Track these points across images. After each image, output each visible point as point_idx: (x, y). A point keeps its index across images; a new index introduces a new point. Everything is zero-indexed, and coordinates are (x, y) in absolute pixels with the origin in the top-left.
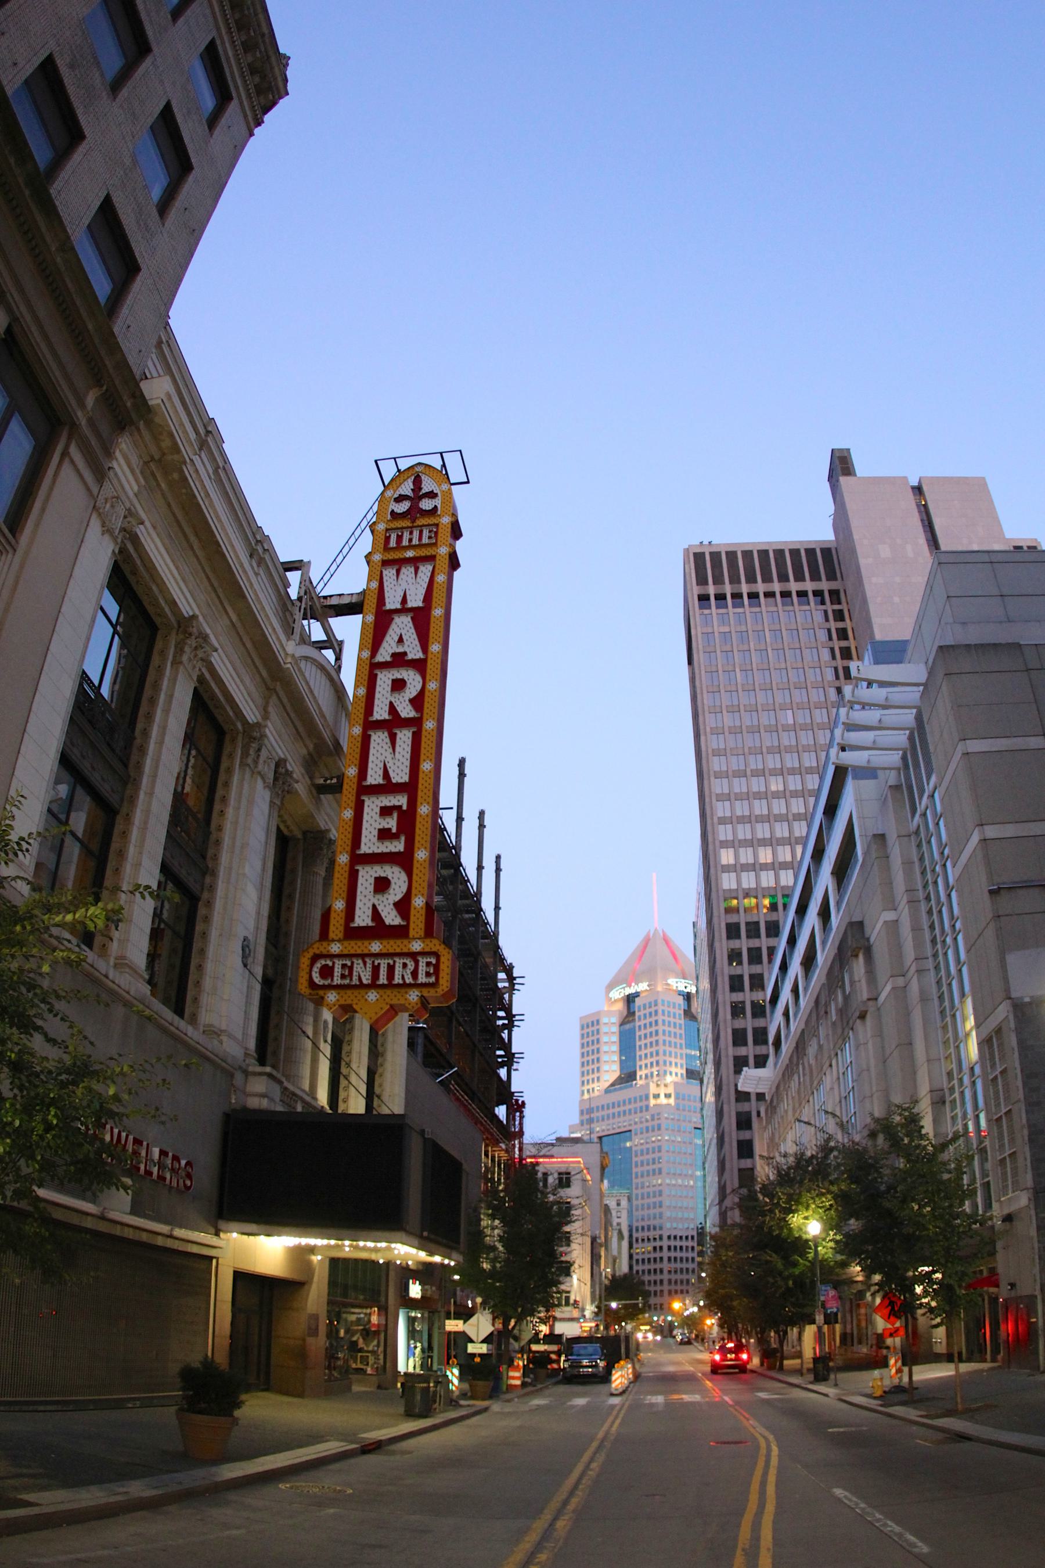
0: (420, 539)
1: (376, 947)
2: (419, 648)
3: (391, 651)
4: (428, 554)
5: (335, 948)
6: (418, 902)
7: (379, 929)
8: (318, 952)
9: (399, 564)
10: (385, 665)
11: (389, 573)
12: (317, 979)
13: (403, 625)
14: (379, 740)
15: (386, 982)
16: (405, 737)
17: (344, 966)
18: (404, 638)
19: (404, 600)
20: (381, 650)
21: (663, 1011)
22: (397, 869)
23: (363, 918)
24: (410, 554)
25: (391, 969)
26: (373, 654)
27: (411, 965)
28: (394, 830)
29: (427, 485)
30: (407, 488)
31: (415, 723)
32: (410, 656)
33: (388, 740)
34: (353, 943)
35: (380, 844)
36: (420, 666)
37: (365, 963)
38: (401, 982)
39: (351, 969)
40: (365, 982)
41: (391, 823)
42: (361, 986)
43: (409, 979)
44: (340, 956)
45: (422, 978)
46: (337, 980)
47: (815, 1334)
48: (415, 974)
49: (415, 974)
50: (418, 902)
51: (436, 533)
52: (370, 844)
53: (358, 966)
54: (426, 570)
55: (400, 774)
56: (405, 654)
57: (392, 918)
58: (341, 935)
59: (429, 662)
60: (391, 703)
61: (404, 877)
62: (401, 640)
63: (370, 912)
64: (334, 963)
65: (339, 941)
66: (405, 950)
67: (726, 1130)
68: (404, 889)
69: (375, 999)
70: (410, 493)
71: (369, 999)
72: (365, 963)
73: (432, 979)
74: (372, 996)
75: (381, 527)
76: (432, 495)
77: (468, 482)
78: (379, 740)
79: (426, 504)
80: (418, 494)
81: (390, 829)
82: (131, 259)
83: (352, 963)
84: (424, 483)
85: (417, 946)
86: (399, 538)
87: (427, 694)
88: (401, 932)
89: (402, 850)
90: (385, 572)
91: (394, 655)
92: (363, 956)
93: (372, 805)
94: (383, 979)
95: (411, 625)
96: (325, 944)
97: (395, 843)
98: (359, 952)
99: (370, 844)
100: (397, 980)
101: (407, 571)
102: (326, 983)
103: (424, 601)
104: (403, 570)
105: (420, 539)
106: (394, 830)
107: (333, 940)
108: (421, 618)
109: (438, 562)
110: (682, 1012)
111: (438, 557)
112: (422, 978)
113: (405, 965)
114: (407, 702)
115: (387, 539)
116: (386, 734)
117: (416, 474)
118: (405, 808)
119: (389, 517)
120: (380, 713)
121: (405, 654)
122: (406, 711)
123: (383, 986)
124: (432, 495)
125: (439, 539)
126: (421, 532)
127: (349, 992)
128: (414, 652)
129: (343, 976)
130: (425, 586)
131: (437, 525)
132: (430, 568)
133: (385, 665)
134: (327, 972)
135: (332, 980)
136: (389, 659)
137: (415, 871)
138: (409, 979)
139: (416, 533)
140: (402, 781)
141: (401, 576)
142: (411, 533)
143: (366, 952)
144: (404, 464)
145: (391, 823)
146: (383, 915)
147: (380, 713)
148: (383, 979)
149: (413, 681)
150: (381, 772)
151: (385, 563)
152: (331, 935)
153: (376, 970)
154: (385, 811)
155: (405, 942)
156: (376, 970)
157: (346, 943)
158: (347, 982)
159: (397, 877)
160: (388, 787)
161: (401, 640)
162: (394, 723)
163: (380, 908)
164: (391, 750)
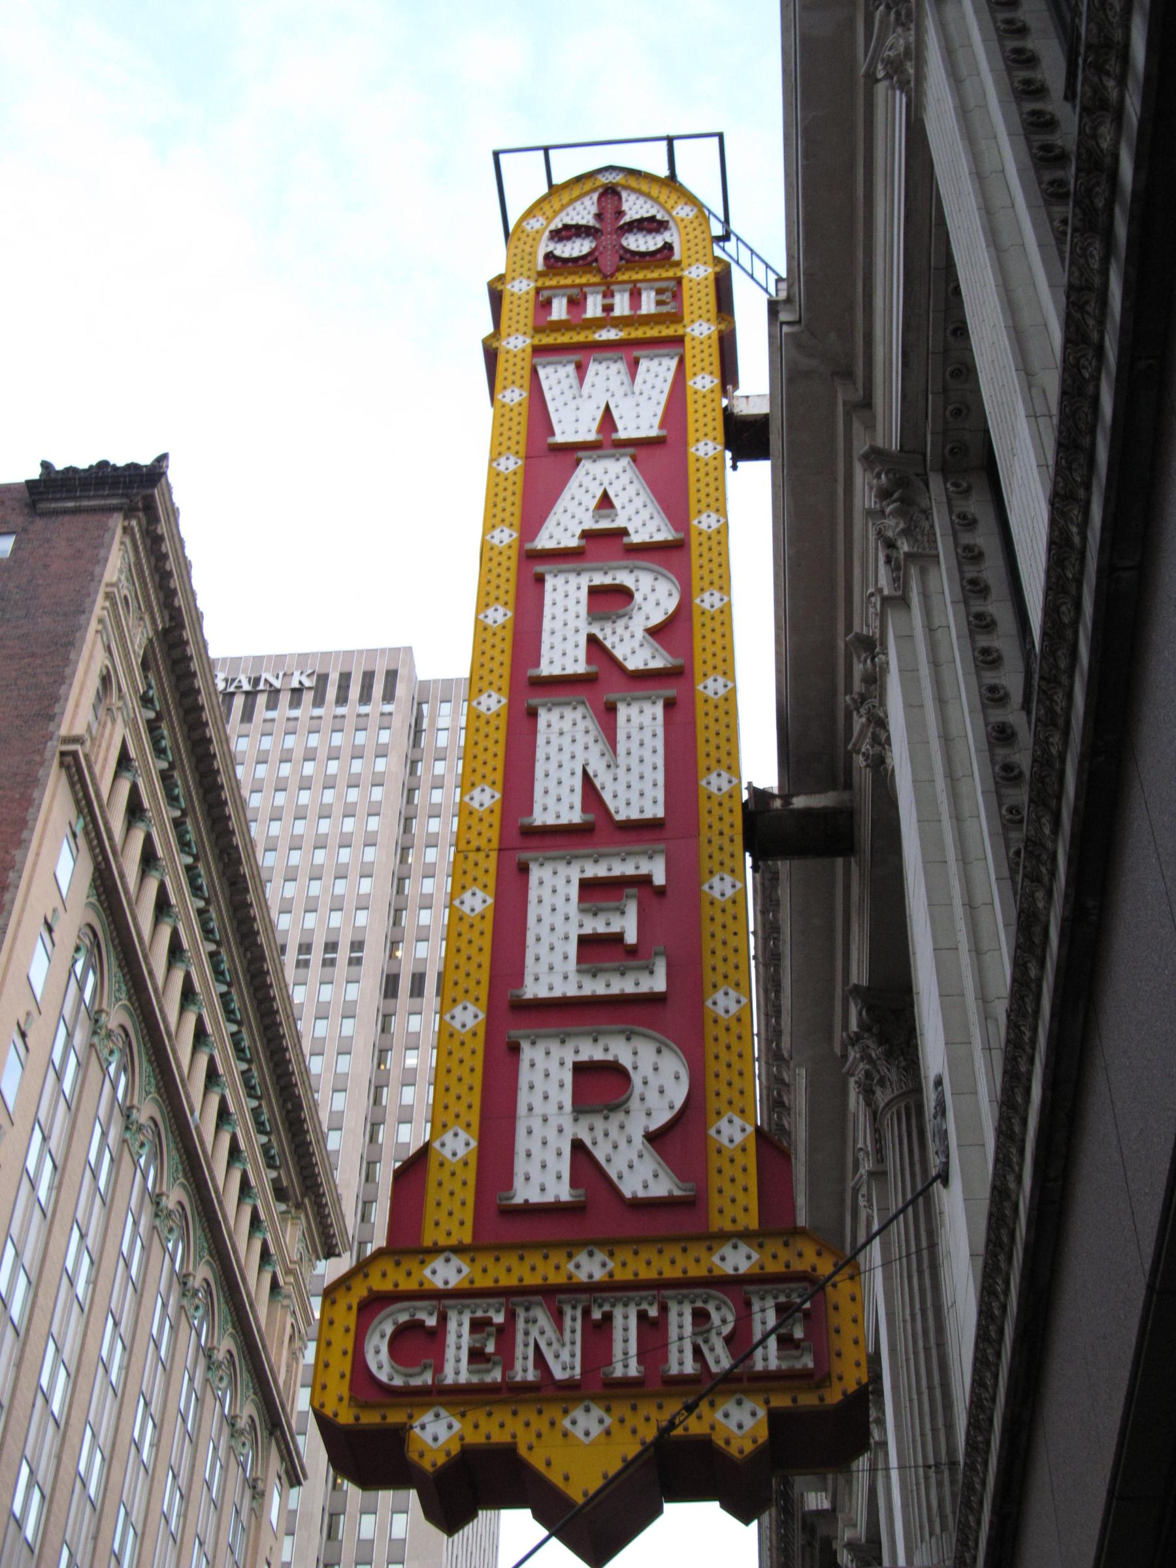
1: (590, 1267)
5: (445, 1273)
6: (732, 1132)
12: (380, 1362)
15: (633, 1370)
26: (533, 515)
27: (723, 1319)
28: (631, 938)
29: (635, 207)
33: (591, 724)
36: (669, 555)
37: (558, 1318)
39: (505, 1334)
40: (559, 1374)
46: (457, 1368)
50: (732, 1132)
52: (552, 971)
55: (637, 793)
57: (640, 1175)
74: (587, 1422)
77: (720, 136)
80: (610, 221)
82: (84, 471)
85: (736, 1260)
88: (677, 1218)
90: (542, 373)
92: (554, 1296)
94: (626, 1362)
96: (409, 1263)
99: (552, 971)
100: (681, 1362)
106: (631, 938)
112: (769, 1358)
113: (700, 1316)
117: (608, 187)
120: (563, 653)
122: (633, 649)
123: (514, 760)
135: (439, 1369)
136: (574, 543)
138: (720, 1359)
143: (555, 1279)
144: (566, 167)
148: (626, 1362)
149: (655, 597)
153: (598, 1334)
157: (486, 1260)
158: (496, 1375)
159: (659, 1080)
160: (597, 828)
162: (600, 686)
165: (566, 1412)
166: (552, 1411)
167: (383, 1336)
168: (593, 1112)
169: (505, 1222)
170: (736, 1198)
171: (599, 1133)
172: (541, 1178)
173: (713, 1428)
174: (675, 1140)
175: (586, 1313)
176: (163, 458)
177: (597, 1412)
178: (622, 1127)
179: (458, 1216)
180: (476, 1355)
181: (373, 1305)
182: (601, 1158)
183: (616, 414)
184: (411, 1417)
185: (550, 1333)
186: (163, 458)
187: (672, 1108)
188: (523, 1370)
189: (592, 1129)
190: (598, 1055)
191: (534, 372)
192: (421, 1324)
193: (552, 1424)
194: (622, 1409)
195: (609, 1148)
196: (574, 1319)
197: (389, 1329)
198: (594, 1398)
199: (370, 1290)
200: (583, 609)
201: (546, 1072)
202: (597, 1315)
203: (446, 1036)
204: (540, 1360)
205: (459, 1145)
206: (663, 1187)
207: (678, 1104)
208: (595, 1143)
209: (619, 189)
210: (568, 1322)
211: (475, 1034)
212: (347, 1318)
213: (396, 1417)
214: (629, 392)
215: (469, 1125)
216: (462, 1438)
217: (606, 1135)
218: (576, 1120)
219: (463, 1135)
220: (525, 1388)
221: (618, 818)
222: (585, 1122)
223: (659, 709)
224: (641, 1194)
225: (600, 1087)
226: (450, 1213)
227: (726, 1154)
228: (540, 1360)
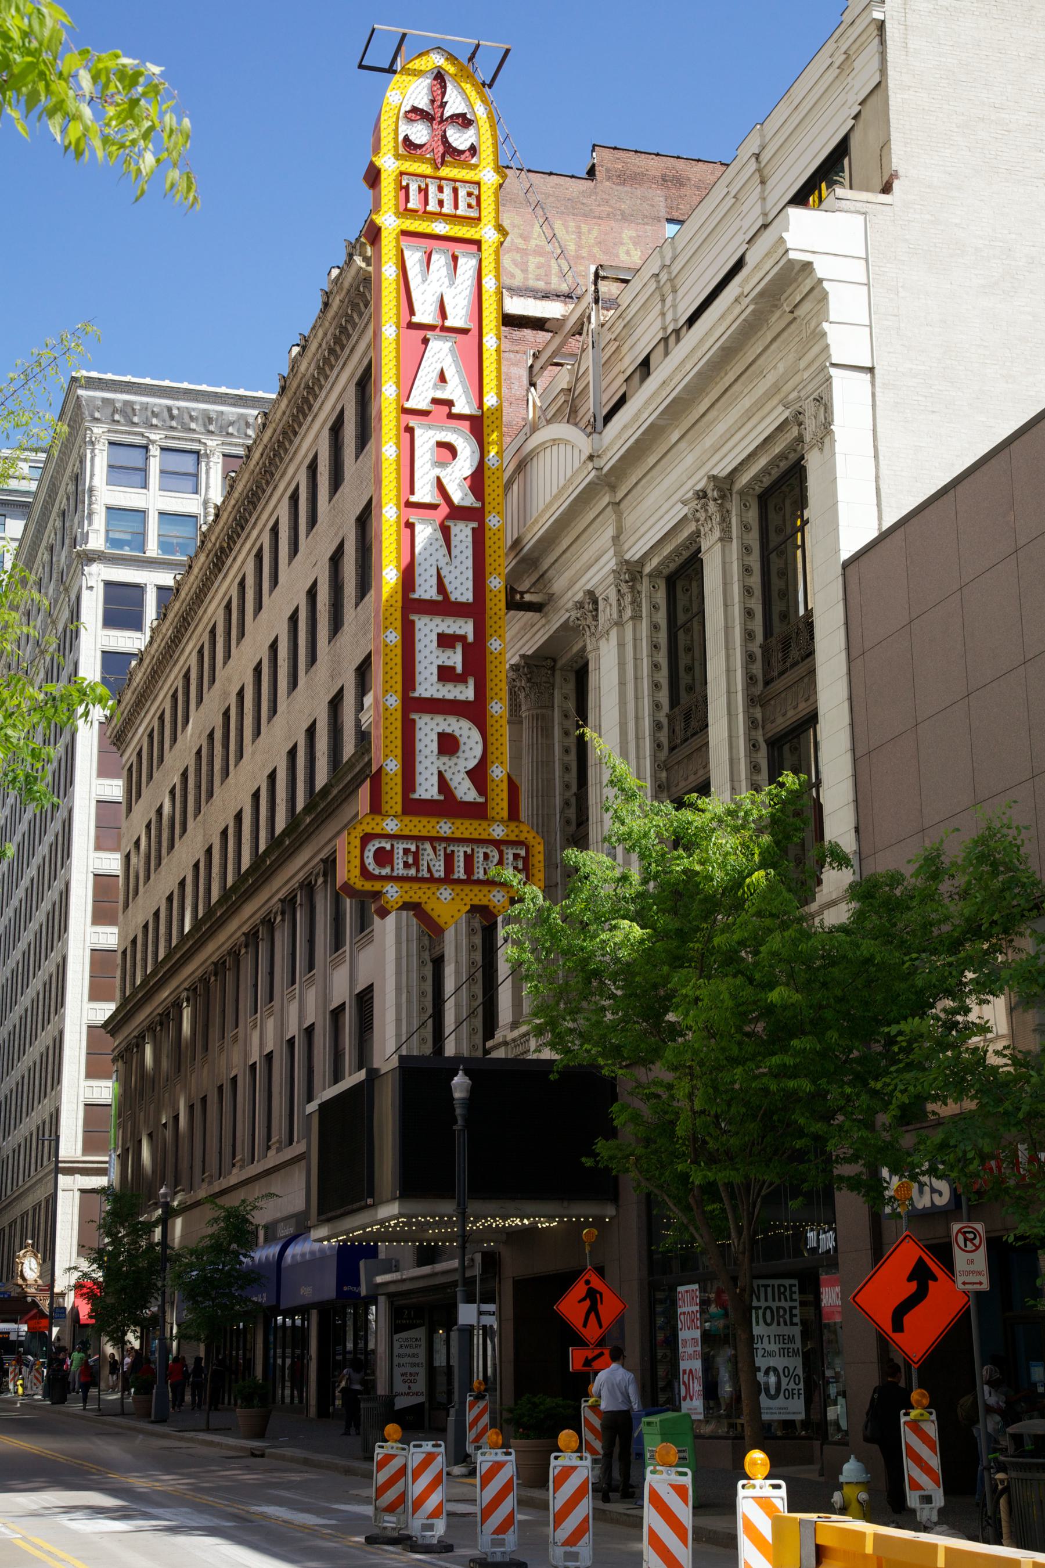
5: (391, 826)
6: (498, 772)
7: (447, 805)
23: (427, 789)
24: (440, 228)
28: (459, 669)
35: (440, 686)
39: (416, 855)
41: (455, 659)
42: (432, 880)
52: (428, 686)
57: (465, 791)
61: (476, 735)
66: (485, 836)
71: (442, 897)
74: (445, 893)
85: (498, 832)
94: (460, 873)
96: (378, 818)
97: (461, 687)
99: (428, 686)
134: (383, 857)
142: (441, 189)
143: (433, 834)
145: (455, 659)
148: (460, 873)
152: (385, 808)
153: (449, 859)
154: (445, 641)
155: (485, 824)
156: (449, 859)
158: (412, 872)
170: (500, 804)
174: (478, 775)
176: (372, 985)
180: (406, 865)
183: (448, 776)
186: (372, 985)
190: (449, 730)
197: (373, 849)
201: (429, 729)
204: (429, 870)
209: (446, 78)
213: (377, 886)
220: (423, 880)
223: (470, 533)
225: (448, 745)
228: (429, 870)
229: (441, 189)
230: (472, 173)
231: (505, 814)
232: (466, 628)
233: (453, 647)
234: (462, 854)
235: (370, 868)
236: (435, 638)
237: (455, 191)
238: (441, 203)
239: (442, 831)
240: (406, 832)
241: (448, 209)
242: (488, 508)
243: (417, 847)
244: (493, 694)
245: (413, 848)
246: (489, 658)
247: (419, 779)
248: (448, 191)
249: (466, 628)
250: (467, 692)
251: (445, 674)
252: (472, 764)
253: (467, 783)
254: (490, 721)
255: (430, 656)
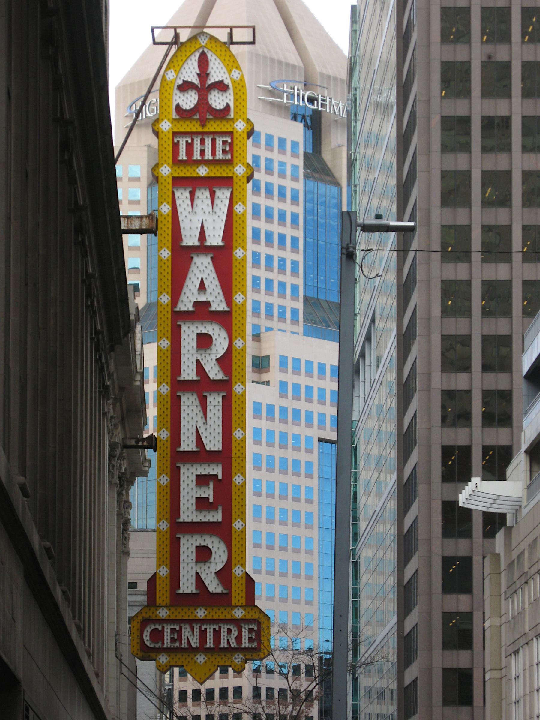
0: (214, 153)
1: (201, 613)
2: (221, 297)
3: (194, 300)
4: (224, 175)
5: (163, 613)
7: (202, 596)
8: (147, 616)
9: (194, 184)
10: (188, 316)
11: (183, 196)
13: (202, 268)
14: (189, 403)
16: (215, 401)
17: (173, 630)
18: (207, 283)
19: (202, 236)
20: (183, 297)
21: (257, 303)
22: (216, 540)
23: (187, 585)
24: (203, 171)
25: (217, 634)
27: (235, 633)
30: (190, 72)
31: (225, 387)
32: (214, 307)
33: (197, 403)
34: (179, 609)
35: (198, 513)
36: (225, 319)
37: (192, 629)
38: (226, 646)
39: (180, 632)
40: (194, 645)
41: (208, 493)
42: (191, 650)
43: (234, 644)
44: (168, 621)
45: (245, 643)
47: (228, 33)
48: (239, 639)
49: (239, 639)
51: (231, 145)
52: (188, 513)
53: (186, 632)
54: (223, 196)
56: (208, 304)
57: (214, 586)
58: (167, 601)
59: (234, 315)
60: (198, 361)
61: (223, 547)
62: (202, 287)
63: (193, 580)
64: (163, 627)
65: (166, 606)
66: (228, 617)
67: (421, 369)
68: (225, 558)
69: (203, 661)
70: (196, 80)
71: (199, 661)
72: (192, 629)
73: (255, 645)
75: (165, 126)
76: (221, 86)
77: (253, 43)
78: (189, 403)
79: (217, 100)
81: (208, 498)
83: (181, 627)
84: (211, 65)
85: (239, 613)
86: (190, 147)
87: (234, 354)
89: (220, 520)
90: (177, 194)
91: (197, 304)
92: (191, 622)
93: (188, 474)
94: (210, 643)
95: (211, 267)
96: (153, 609)
97: (213, 513)
98: (186, 617)
99: (188, 513)
100: (223, 644)
101: (203, 195)
102: (157, 646)
103: (223, 240)
104: (198, 194)
105: (214, 153)
107: (160, 606)
108: (223, 258)
109: (235, 186)
110: (300, 162)
111: (235, 180)
112: (245, 643)
113: (229, 631)
114: (214, 361)
115: (176, 146)
116: (195, 396)
118: (220, 477)
119: (174, 115)
121: (208, 304)
122: (214, 372)
124: (221, 86)
125: (235, 154)
126: (214, 141)
127: (179, 655)
128: (218, 304)
129: (173, 640)
130: (224, 218)
131: (231, 134)
132: (228, 194)
133: (188, 316)
134: (157, 635)
135: (163, 643)
137: (234, 543)
138: (234, 644)
139: (208, 141)
140: (216, 449)
141: (196, 202)
142: (202, 142)
143: (192, 617)
145: (208, 493)
146: (206, 582)
147: (188, 372)
148: (210, 643)
150: (194, 438)
151: (178, 182)
152: (159, 601)
153: (203, 634)
154: (202, 480)
155: (228, 609)
156: (203, 634)
157: (173, 609)
158: (177, 644)
160: (201, 455)
161: (202, 287)
163: (203, 576)
164: (201, 414)
165: (198, 167)
166: (194, 168)
167: (147, 631)
168: (202, 562)
169: (179, 600)
171: (202, 570)
172: (187, 585)
173: (233, 129)
175: (200, 627)
177: (205, 168)
178: (209, 567)
179: (167, 277)
181: (145, 622)
182: (203, 578)
184: (156, 656)
185: (191, 633)
187: (223, 562)
188: (184, 645)
189: (201, 568)
190: (204, 331)
191: (173, 193)
192: (158, 629)
193: (192, 659)
194: (209, 655)
195: (206, 362)
196: (197, 629)
197: (150, 630)
198: (202, 652)
199: (143, 617)
200: (195, 344)
201: (188, 545)
202: (203, 629)
203: (160, 350)
205: (164, 572)
206: (219, 589)
207: (225, 561)
208: (202, 359)
210: (195, 630)
211: (168, 305)
212: (137, 625)
214: (211, 212)
215: (167, 337)
216: (172, 129)
217: (205, 570)
218: (196, 565)
219: (167, 296)
220: (184, 649)
221: (208, 449)
222: (200, 565)
223: (220, 399)
224: (215, 378)
226: (163, 595)
227: (238, 261)
229: (202, 142)
230: (228, 125)
231: (243, 601)
232: (217, 470)
233: (208, 485)
234: (212, 630)
235: (148, 643)
236: (194, 478)
237: (214, 141)
238: (202, 152)
239: (199, 615)
240: (173, 617)
241: (208, 156)
242: (234, 380)
243: (181, 627)
244: (238, 161)
245: (178, 628)
246: (235, 263)
247: (183, 367)
248: (208, 141)
249: (217, 470)
250: (217, 516)
251: (202, 504)
252: (220, 567)
253: (217, 368)
254: (234, 328)
255: (189, 492)
